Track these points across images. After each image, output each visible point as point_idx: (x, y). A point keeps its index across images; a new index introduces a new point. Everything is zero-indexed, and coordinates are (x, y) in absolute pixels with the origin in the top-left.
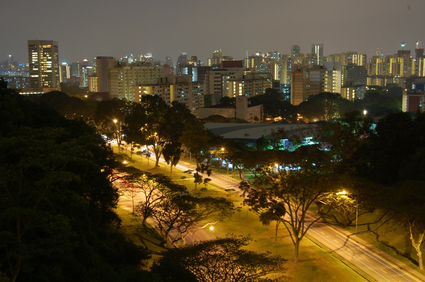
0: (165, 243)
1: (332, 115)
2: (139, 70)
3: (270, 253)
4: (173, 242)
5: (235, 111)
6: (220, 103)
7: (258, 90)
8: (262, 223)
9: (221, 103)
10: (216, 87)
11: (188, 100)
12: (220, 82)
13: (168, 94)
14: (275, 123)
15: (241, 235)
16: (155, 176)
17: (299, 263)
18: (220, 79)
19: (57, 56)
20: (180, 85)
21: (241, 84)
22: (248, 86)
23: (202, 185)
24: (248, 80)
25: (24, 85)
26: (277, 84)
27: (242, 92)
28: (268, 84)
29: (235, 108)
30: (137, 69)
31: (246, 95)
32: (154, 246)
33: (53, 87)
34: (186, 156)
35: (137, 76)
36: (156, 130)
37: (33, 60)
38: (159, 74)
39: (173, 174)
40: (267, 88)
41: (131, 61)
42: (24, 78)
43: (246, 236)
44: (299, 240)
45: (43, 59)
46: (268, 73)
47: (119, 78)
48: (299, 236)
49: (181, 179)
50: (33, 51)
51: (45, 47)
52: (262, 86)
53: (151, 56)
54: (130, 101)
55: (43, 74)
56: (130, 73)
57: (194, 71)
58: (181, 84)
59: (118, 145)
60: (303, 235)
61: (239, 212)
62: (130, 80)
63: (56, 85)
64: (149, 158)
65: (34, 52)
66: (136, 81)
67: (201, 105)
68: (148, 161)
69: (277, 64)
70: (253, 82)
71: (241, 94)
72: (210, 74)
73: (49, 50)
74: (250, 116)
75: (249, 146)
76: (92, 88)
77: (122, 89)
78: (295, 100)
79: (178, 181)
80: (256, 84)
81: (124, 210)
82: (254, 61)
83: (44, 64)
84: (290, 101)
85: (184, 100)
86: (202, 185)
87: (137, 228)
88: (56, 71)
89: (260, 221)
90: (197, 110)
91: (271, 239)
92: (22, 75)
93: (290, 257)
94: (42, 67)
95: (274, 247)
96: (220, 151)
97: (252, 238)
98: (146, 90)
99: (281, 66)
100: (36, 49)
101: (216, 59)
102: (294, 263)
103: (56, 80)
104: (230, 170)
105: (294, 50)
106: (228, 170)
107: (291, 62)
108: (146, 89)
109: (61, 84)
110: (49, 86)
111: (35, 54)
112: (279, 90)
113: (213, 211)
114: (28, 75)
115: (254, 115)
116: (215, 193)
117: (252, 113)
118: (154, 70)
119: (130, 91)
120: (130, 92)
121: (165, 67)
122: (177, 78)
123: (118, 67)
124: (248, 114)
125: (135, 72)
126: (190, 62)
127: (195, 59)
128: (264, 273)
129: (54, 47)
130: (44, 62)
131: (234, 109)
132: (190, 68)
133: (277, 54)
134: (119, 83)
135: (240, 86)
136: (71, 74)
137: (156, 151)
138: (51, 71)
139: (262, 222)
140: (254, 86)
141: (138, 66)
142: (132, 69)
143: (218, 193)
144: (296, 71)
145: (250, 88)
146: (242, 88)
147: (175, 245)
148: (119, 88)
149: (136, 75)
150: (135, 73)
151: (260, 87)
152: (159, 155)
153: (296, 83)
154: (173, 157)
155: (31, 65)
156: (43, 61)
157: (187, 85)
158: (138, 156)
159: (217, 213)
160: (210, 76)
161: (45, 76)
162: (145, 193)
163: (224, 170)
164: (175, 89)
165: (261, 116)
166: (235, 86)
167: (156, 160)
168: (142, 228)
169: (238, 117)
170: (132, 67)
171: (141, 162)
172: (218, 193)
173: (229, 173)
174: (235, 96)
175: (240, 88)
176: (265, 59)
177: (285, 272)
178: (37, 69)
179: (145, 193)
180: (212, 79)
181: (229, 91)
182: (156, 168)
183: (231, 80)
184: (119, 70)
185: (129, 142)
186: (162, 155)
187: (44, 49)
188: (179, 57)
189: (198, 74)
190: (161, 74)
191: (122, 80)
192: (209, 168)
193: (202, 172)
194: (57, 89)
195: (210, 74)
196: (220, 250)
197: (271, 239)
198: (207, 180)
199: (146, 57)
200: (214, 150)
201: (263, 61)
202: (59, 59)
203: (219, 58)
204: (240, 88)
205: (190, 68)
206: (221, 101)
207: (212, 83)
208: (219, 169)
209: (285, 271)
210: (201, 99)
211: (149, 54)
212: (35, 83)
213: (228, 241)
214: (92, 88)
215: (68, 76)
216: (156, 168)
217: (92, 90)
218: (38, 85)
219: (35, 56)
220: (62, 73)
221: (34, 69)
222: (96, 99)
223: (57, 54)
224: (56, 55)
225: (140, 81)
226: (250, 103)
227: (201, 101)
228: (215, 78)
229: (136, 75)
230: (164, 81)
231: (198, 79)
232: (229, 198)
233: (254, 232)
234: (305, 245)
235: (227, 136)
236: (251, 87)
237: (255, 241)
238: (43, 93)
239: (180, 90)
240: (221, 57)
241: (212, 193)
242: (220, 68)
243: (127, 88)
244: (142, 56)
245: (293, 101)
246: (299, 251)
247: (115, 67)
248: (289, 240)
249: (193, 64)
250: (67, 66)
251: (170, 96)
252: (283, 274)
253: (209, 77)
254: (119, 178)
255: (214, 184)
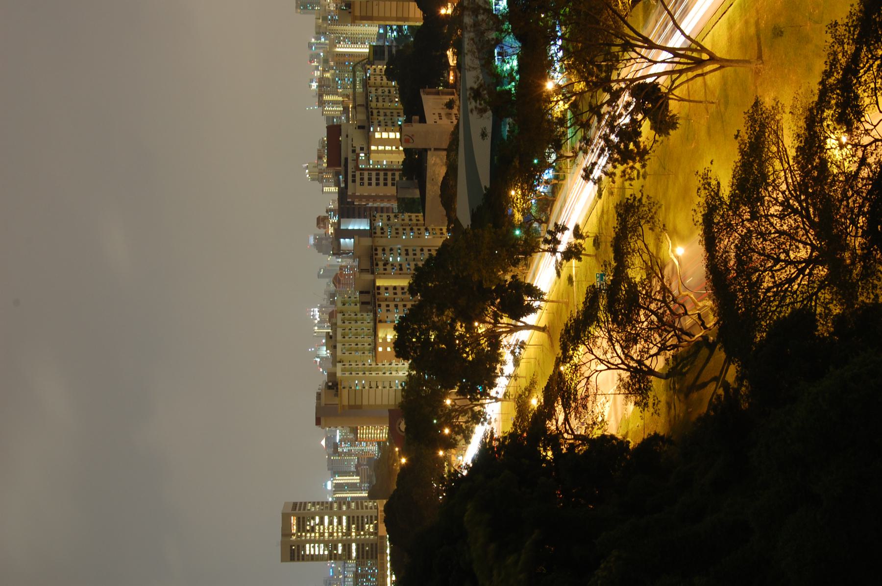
0: (708, 339)
1: (447, 69)
2: (344, 345)
3: (738, 133)
4: (705, 328)
5: (432, 149)
6: (416, 181)
7: (389, 96)
8: (672, 130)
9: (416, 179)
10: (382, 181)
12: (371, 174)
14: (459, 66)
15: (698, 192)
16: (565, 349)
17: (764, 58)
19: (314, 504)
20: (377, 265)
21: (376, 134)
22: (381, 118)
23: (587, 244)
24: (368, 118)
25: (372, 569)
26: (377, 53)
27: (392, 131)
28: (378, 75)
29: (426, 150)
30: (342, 351)
31: (400, 123)
33: (376, 515)
35: (356, 351)
37: (321, 553)
38: (353, 305)
39: (562, 299)
40: (384, 78)
42: (357, 569)
44: (713, 59)
45: (319, 532)
46: (354, 67)
47: (360, 388)
48: (705, 57)
49: (572, 285)
50: (303, 552)
51: (295, 527)
52: (381, 89)
53: (316, 310)
54: (407, 376)
55: (350, 535)
59: (499, 403)
60: (703, 49)
61: (648, 177)
62: (364, 364)
63: (373, 508)
64: (527, 344)
65: (305, 551)
66: (366, 352)
67: (418, 220)
68: (532, 347)
69: (336, 46)
70: (371, 108)
71: (398, 135)
72: (354, 194)
73: (301, 520)
74: (444, 117)
76: (381, 435)
77: (383, 382)
78: (411, 15)
79: (579, 299)
80: (378, 101)
82: (328, 94)
83: (330, 531)
84: (418, 26)
85: (407, 257)
87: (672, 392)
88: (344, 508)
89: (668, 134)
92: (351, 573)
93: (750, 77)
94: (335, 534)
95: (726, 109)
96: (516, 198)
97: (705, 169)
99: (339, 37)
100: (298, 546)
102: (764, 70)
103: (362, 508)
104: (556, 177)
105: (305, 8)
107: (332, 17)
108: (384, 336)
109: (372, 496)
110: (375, 522)
111: (309, 549)
112: (390, 47)
113: (643, 241)
114: (352, 563)
115: (443, 109)
116: (605, 216)
118: (344, 315)
119: (387, 365)
121: (339, 283)
122: (362, 271)
123: (337, 388)
124: (439, 122)
127: (322, 221)
128: (782, 155)
129: (295, 510)
130: (326, 531)
131: (429, 153)
133: (314, 44)
135: (379, 136)
137: (514, 329)
138: (344, 518)
139: (671, 132)
140: (380, 104)
141: (335, 347)
143: (605, 209)
144: (350, 12)
145: (385, 115)
146: (386, 131)
147: (712, 324)
148: (380, 388)
151: (383, 93)
153: (375, 14)
155: (332, 556)
156: (324, 532)
157: (376, 250)
158: (523, 363)
160: (359, 194)
161: (353, 530)
162: (601, 371)
164: (385, 275)
165: (444, 93)
166: (381, 148)
167: (531, 331)
170: (338, 359)
171: (536, 358)
172: (605, 209)
174: (401, 148)
175: (385, 135)
176: (324, 71)
177: (783, 106)
178: (340, 545)
179: (601, 371)
180: (365, 191)
181: (391, 160)
182: (548, 331)
183: (368, 153)
184: (344, 388)
185: (492, 385)
187: (298, 530)
188: (319, 252)
189: (355, 218)
190: (353, 298)
191: (363, 382)
193: (559, 242)
194: (381, 508)
195: (354, 194)
196: (728, 244)
197: (709, 112)
199: (319, 319)
200: (513, 211)
201: (328, 75)
202: (321, 500)
203: (321, 169)
204: (385, 135)
206: (410, 178)
207: (373, 190)
209: (780, 107)
210: (407, 221)
211: (312, 313)
212: (367, 551)
213: (708, 221)
214: (381, 435)
215: (356, 479)
216: (548, 331)
217: (384, 435)
218: (372, 545)
219: (312, 550)
220: (350, 491)
221: (340, 552)
222: (399, 428)
223: (310, 504)
224: (311, 507)
225: (366, 345)
226: (417, 118)
227: (411, 220)
228: (363, 185)
229: (353, 352)
230: (367, 298)
231: (365, 217)
233: (693, 146)
234: (726, 38)
235: (485, 180)
236: (382, 112)
237: (711, 163)
238: (388, 536)
239: (388, 264)
240: (320, 165)
242: (343, 172)
244: (316, 328)
245: (416, 20)
246: (741, 58)
247: (336, 395)
248: (714, 78)
249: (333, 224)
250: (335, 482)
252: (787, 110)
253: (361, 197)
254: (566, 420)
255: (586, 215)
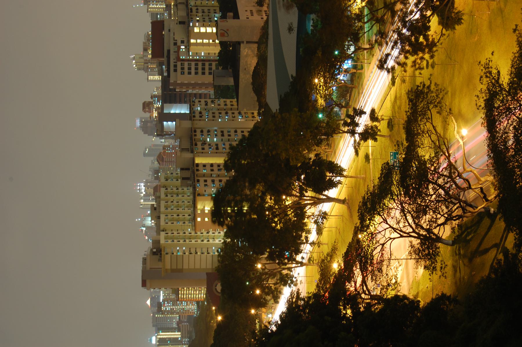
0: (489, 210)
3: (517, 27)
4: (487, 200)
5: (245, 42)
9: (230, 69)
11: (222, 130)
12: (191, 64)
13: (212, 168)
15: (480, 80)
16: (362, 219)
18: (186, 64)
20: (196, 145)
21: (195, 28)
23: (382, 126)
24: (188, 15)
27: (209, 26)
29: (239, 43)
30: (165, 221)
31: (216, 19)
32: (492, 232)
34: (327, 144)
36: (278, 201)
38: (175, 180)
39: (360, 175)
41: (149, 222)
43: (482, 70)
47: (181, 254)
49: (369, 162)
53: (142, 184)
56: (172, 233)
57: (171, 108)
58: (194, 143)
59: (304, 267)
61: (436, 66)
67: (232, 105)
71: (215, 30)
72: (175, 82)
74: (255, 14)
75: (311, 28)
76: (200, 296)
77: (202, 248)
81: (422, 275)
85: (222, 138)
86: (382, 126)
87: (457, 257)
89: (454, 28)
90: (243, 112)
91: (489, 9)
97: (487, 59)
98: (203, 208)
101: (148, 66)
104: (355, 67)
106: (354, 71)
113: (432, 123)
115: (254, 6)
117: (251, 11)
119: (205, 234)
120: (208, 234)
121: (163, 161)
123: (161, 254)
124: (251, 18)
125: (169, 223)
126: (154, 115)
127: (147, 106)
131: (242, 45)
132: (164, 117)
134: (191, 253)
135: (198, 31)
136: (172, 330)
137: (316, 202)
139: (457, 27)
141: (159, 217)
142: (164, 228)
143: (398, 96)
145: (203, 12)
146: (203, 26)
147: (493, 196)
148: (199, 253)
149: (175, 222)
150: (172, 223)
152: (325, 197)
154: (328, 174)
157: (195, 131)
158: (325, 232)
159: (438, 121)
160: (180, 82)
162: (394, 239)
163: (355, 76)
164: (203, 153)
166: (199, 41)
168: (459, 247)
169: (256, 39)
170: (162, 228)
171: (337, 228)
172: (398, 96)
173: (362, 68)
174: (217, 41)
175: (203, 30)
179: (394, 239)
180: (185, 79)
181: (209, 52)
182: (348, 204)
183: (188, 46)
184: (167, 254)
185: (298, 251)
186: (326, 193)
188: (144, 133)
190: (174, 174)
191: (184, 248)
192: (351, 113)
193: (357, 125)
195: (175, 82)
197: (491, 8)
198: (373, 116)
199: (144, 193)
200: (316, 97)
204: (203, 30)
205: (164, 117)
208: (353, 86)
210: (222, 106)
213: (489, 106)
214: (200, 296)
215: (177, 335)
217: (202, 296)
222: (216, 289)
225: (186, 215)
226: (231, 14)
227: (226, 105)
228: (184, 74)
229: (175, 222)
230: (187, 174)
231: (185, 102)
232: (408, 78)
233: (476, 39)
235: (292, 70)
236: (200, 9)
237: (492, 54)
241: (398, 108)
242: (166, 63)
243: (200, 239)
244: (142, 201)
247: (160, 260)
249: (157, 109)
250: (158, 337)
251: (216, 163)
253: (182, 85)
254: (364, 282)
255: (381, 100)
